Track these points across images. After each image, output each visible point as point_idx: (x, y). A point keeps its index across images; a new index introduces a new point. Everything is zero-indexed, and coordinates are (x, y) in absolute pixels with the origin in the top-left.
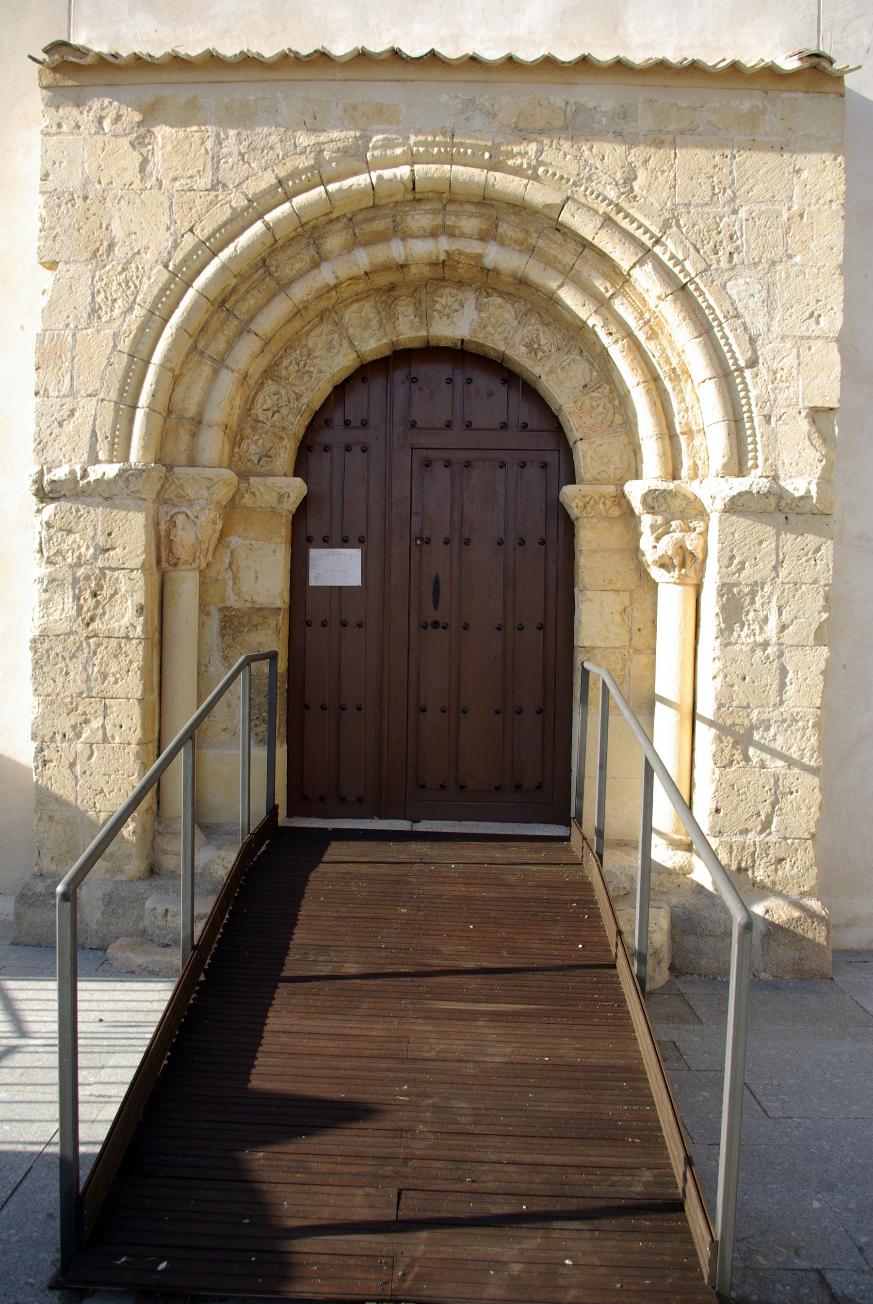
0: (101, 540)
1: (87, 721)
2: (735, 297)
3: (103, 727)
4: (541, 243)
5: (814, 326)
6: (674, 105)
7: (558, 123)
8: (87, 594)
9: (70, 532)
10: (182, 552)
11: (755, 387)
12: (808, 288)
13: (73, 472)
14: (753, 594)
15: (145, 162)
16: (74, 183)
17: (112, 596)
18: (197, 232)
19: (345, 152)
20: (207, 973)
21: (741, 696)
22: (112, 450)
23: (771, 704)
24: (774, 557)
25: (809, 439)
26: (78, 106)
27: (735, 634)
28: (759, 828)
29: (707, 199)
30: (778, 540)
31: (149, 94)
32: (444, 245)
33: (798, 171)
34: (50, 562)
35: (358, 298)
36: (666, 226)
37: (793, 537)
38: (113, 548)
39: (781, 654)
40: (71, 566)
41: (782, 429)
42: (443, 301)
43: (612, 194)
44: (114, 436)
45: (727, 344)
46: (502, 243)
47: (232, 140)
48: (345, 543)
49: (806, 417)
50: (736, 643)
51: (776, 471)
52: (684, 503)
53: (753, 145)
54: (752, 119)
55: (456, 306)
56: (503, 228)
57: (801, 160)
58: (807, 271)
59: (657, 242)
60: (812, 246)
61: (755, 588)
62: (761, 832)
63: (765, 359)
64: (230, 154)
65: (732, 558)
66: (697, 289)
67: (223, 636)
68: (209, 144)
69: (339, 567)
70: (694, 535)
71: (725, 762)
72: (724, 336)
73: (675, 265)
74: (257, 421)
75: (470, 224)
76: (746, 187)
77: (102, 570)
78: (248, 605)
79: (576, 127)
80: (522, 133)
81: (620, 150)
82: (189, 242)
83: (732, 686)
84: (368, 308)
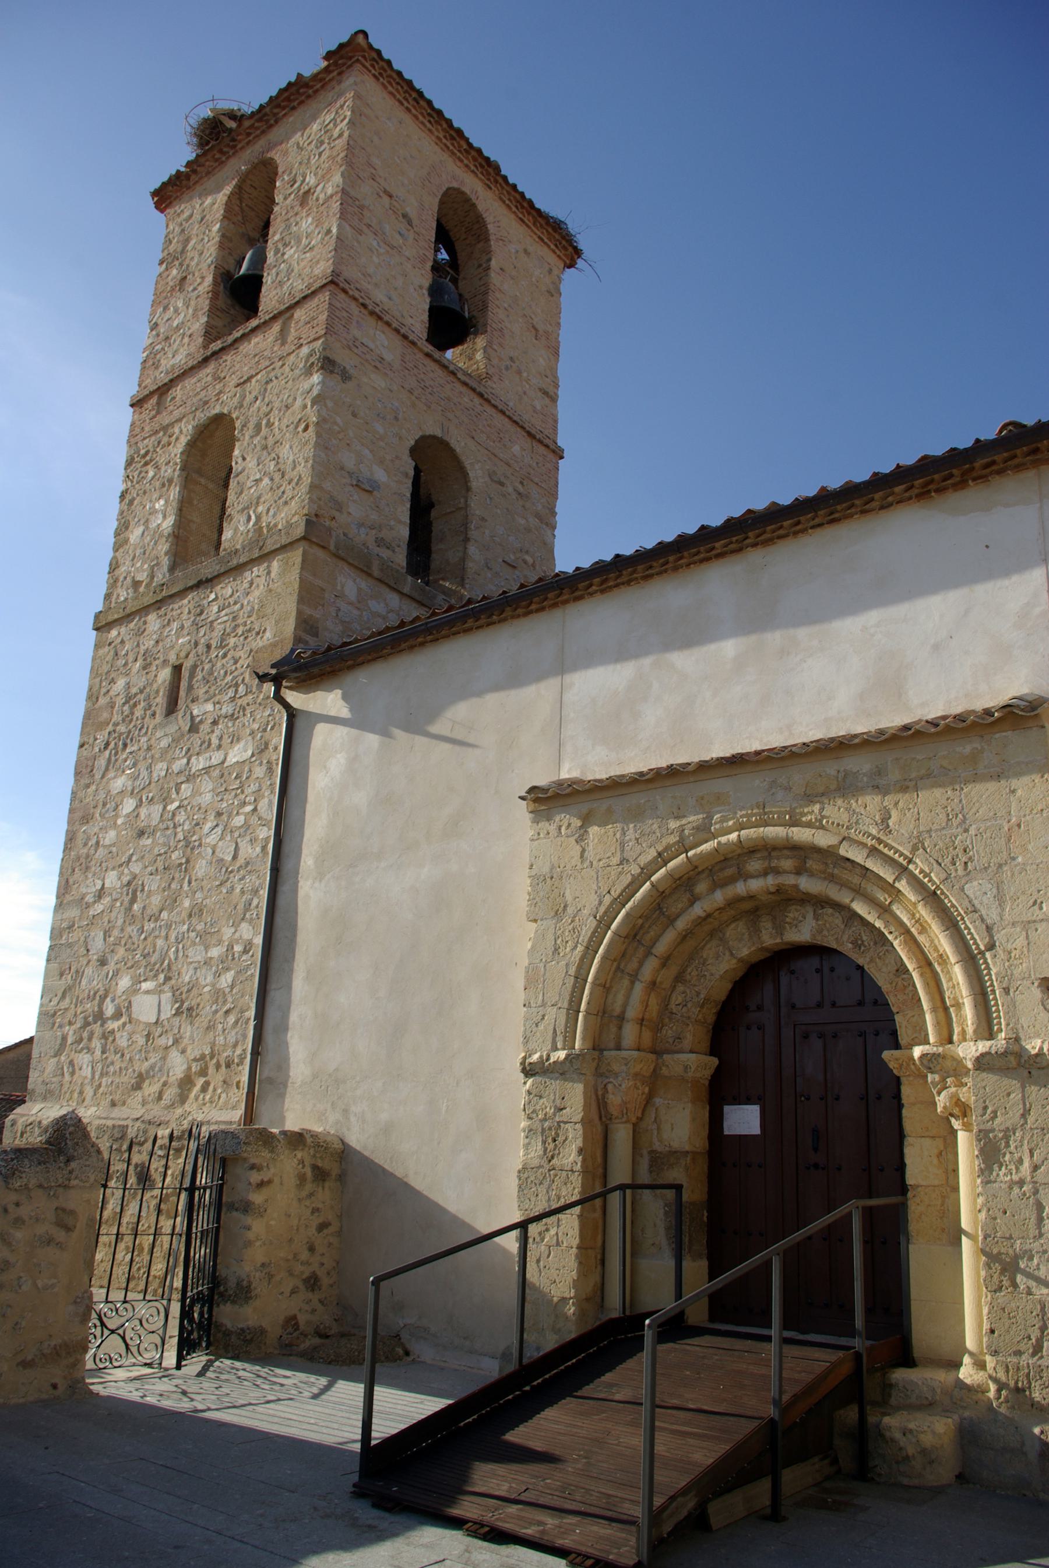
0: (558, 1102)
1: (547, 1230)
2: (972, 896)
3: (557, 1234)
4: (836, 871)
5: (1038, 912)
6: (913, 759)
7: (833, 787)
8: (550, 1140)
9: (541, 1097)
10: (614, 1111)
11: (994, 966)
12: (1030, 882)
13: (541, 1057)
14: (1007, 1138)
15: (583, 851)
16: (546, 870)
17: (564, 1141)
18: (612, 893)
19: (697, 829)
20: (533, 1387)
21: (1004, 1228)
22: (565, 1041)
23: (1031, 1236)
24: (1021, 1106)
25: (1043, 1005)
26: (548, 820)
27: (994, 1174)
28: (1031, 1351)
29: (944, 824)
30: (1023, 1091)
31: (584, 808)
32: (771, 881)
33: (1013, 792)
34: (530, 1118)
35: (735, 919)
36: (914, 849)
37: (1037, 1088)
38: (565, 1108)
39: (1036, 1192)
40: (541, 1121)
41: (1019, 998)
42: (791, 915)
43: (874, 832)
44: (566, 1032)
45: (970, 933)
46: (812, 875)
47: (631, 831)
48: (748, 1101)
49: (1038, 987)
50: (995, 1182)
51: (1017, 1033)
52: (955, 1064)
53: (976, 778)
54: (974, 758)
55: (800, 918)
56: (809, 863)
57: (1015, 783)
58: (1028, 868)
59: (910, 861)
60: (1030, 847)
61: (1008, 1133)
62: (1033, 1355)
63: (1001, 943)
64: (630, 840)
65: (985, 1108)
66: (943, 893)
67: (651, 1172)
68: (618, 835)
69: (744, 1120)
70: (965, 1089)
71: (995, 1287)
72: (967, 928)
73: (925, 877)
74: (672, 1013)
75: (787, 864)
76: (974, 810)
77: (558, 1122)
78: (667, 1149)
79: (846, 787)
80: (810, 798)
81: (878, 798)
82: (607, 900)
83: (995, 1219)
84: (741, 926)
